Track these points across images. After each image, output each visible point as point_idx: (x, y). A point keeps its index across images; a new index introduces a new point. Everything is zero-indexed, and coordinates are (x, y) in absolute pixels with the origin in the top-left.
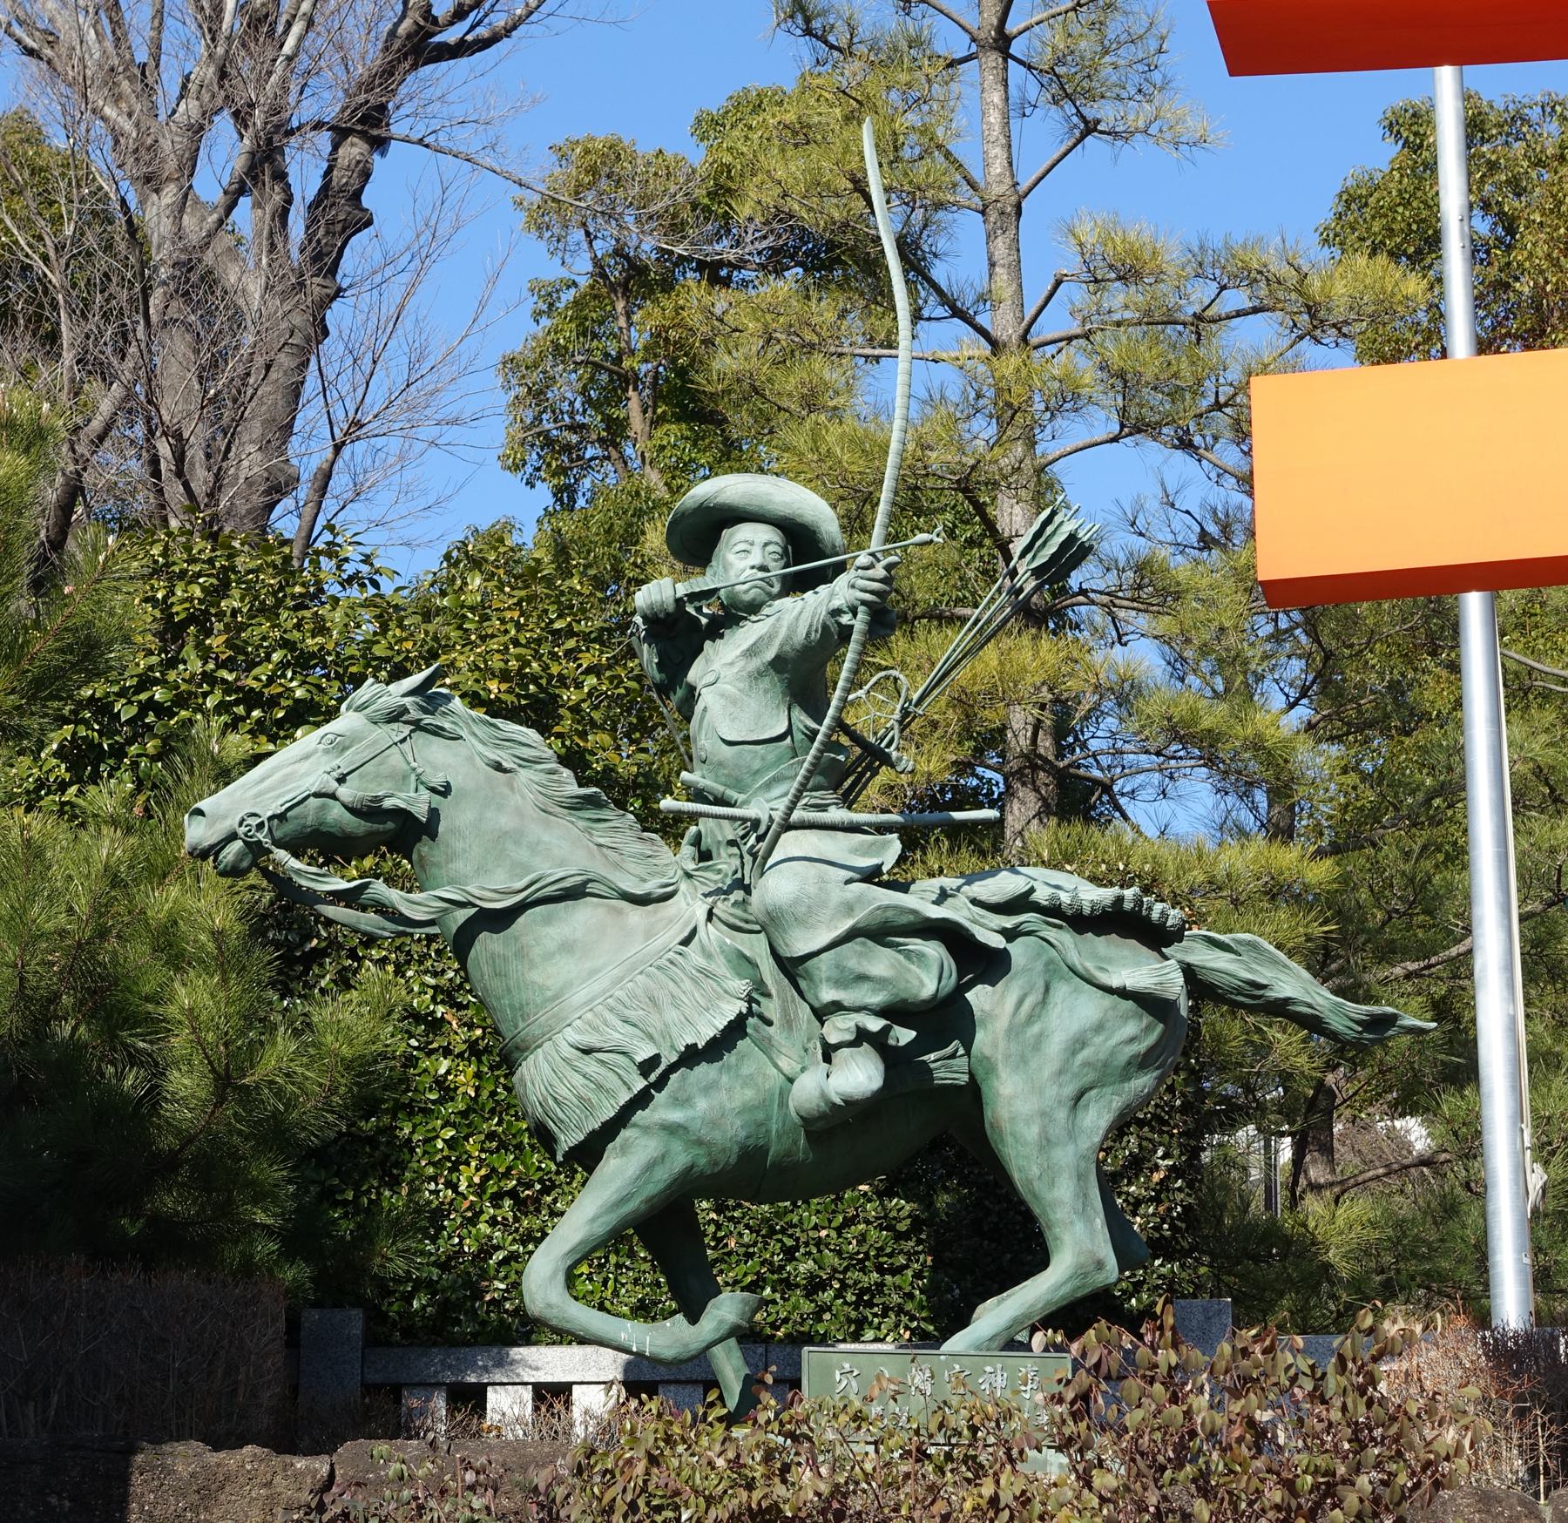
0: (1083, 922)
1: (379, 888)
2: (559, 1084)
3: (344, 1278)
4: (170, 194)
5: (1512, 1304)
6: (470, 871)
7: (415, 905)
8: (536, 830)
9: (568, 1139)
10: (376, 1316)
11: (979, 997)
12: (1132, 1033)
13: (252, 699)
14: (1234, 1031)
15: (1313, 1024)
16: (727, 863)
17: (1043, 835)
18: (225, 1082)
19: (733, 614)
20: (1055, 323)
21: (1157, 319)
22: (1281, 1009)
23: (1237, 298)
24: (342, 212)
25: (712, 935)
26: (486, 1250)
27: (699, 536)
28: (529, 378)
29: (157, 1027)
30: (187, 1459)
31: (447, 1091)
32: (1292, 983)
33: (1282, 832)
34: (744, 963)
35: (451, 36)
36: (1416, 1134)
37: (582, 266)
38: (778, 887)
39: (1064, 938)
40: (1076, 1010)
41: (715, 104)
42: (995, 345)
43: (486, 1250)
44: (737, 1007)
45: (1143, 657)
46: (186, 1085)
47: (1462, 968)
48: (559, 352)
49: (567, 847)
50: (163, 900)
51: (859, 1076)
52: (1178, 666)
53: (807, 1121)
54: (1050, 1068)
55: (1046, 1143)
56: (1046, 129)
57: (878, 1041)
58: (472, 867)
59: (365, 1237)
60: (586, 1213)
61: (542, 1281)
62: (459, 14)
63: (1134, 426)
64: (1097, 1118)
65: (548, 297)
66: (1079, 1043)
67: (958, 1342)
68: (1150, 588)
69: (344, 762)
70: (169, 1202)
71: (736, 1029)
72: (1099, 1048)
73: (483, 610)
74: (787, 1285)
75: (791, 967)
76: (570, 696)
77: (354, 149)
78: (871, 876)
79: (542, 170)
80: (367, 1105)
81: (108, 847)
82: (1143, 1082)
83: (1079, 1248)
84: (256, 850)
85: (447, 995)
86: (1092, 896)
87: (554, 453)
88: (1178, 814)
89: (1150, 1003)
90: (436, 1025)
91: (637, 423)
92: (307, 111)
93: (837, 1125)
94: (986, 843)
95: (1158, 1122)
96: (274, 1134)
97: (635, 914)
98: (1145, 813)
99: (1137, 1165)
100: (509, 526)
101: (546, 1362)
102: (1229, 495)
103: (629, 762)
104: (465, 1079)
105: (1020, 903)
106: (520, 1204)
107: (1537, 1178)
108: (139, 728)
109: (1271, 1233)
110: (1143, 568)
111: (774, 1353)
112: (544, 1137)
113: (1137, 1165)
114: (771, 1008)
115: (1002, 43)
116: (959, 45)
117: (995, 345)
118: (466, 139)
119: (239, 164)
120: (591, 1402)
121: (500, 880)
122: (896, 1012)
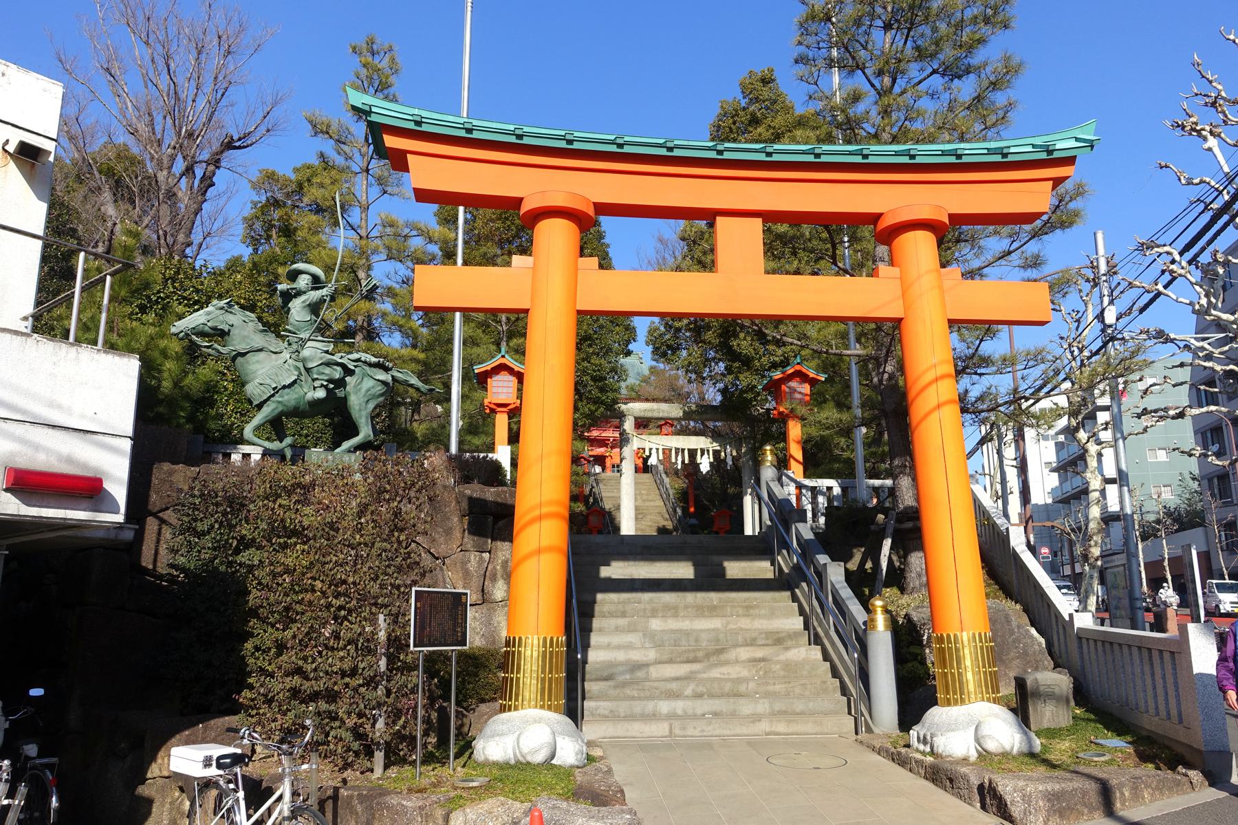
0: (371, 365)
1: (216, 346)
2: (254, 390)
3: (200, 428)
4: (165, 172)
5: (454, 449)
6: (237, 343)
7: (224, 350)
8: (252, 336)
9: (255, 403)
10: (206, 437)
11: (348, 379)
12: (380, 389)
13: (184, 298)
14: (401, 388)
15: (418, 389)
16: (295, 346)
17: (364, 344)
18: (176, 384)
19: (299, 293)
20: (374, 233)
21: (397, 235)
22: (412, 386)
23: (415, 233)
24: (208, 182)
25: (290, 361)
26: (233, 424)
27: (294, 276)
28: (249, 223)
29: (160, 371)
30: (166, 466)
31: (226, 389)
32: (414, 380)
33: (414, 346)
34: (297, 368)
35: (237, 144)
36: (439, 408)
37: (264, 199)
38: (306, 353)
39: (367, 368)
40: (368, 383)
41: (298, 166)
42: (361, 237)
43: (233, 424)
44: (294, 378)
45: (387, 307)
46: (167, 385)
47: (450, 377)
48: (258, 218)
49: (259, 340)
50: (163, 343)
51: (321, 394)
52: (395, 309)
53: (309, 403)
54: (362, 395)
55: (360, 410)
56: (375, 191)
57: (326, 387)
58: (237, 343)
59: (206, 419)
60: (259, 418)
61: (248, 431)
62: (240, 139)
63: (389, 258)
64: (371, 406)
65: (255, 204)
66: (368, 390)
67: (338, 450)
68: (390, 292)
69: (209, 317)
70: (161, 409)
71: (295, 382)
72: (373, 391)
73: (240, 283)
74: (300, 435)
75: (308, 370)
76: (259, 304)
77: (211, 168)
78: (327, 352)
79: (255, 176)
80: (208, 391)
81: (151, 330)
82: (382, 399)
83: (365, 432)
84: (187, 335)
85: (227, 368)
86: (374, 360)
87: (254, 242)
88: (392, 341)
89: (384, 383)
90: (224, 374)
91: (274, 236)
92: (201, 158)
93: (315, 403)
94: (352, 348)
95: (384, 406)
96: (187, 397)
97: (274, 356)
98: (386, 340)
99: (378, 415)
100: (241, 256)
101: (246, 449)
102: (409, 273)
103: (275, 325)
104: (230, 387)
105: (358, 360)
106: (242, 415)
107: (461, 423)
108: (157, 302)
109: (406, 430)
110: (389, 288)
111: (299, 452)
112: (250, 402)
113: (378, 415)
114: (303, 378)
115: (367, 171)
116: (358, 170)
117: (361, 237)
118: (240, 170)
119: (184, 168)
120: (256, 457)
121: (243, 346)
122: (330, 381)
